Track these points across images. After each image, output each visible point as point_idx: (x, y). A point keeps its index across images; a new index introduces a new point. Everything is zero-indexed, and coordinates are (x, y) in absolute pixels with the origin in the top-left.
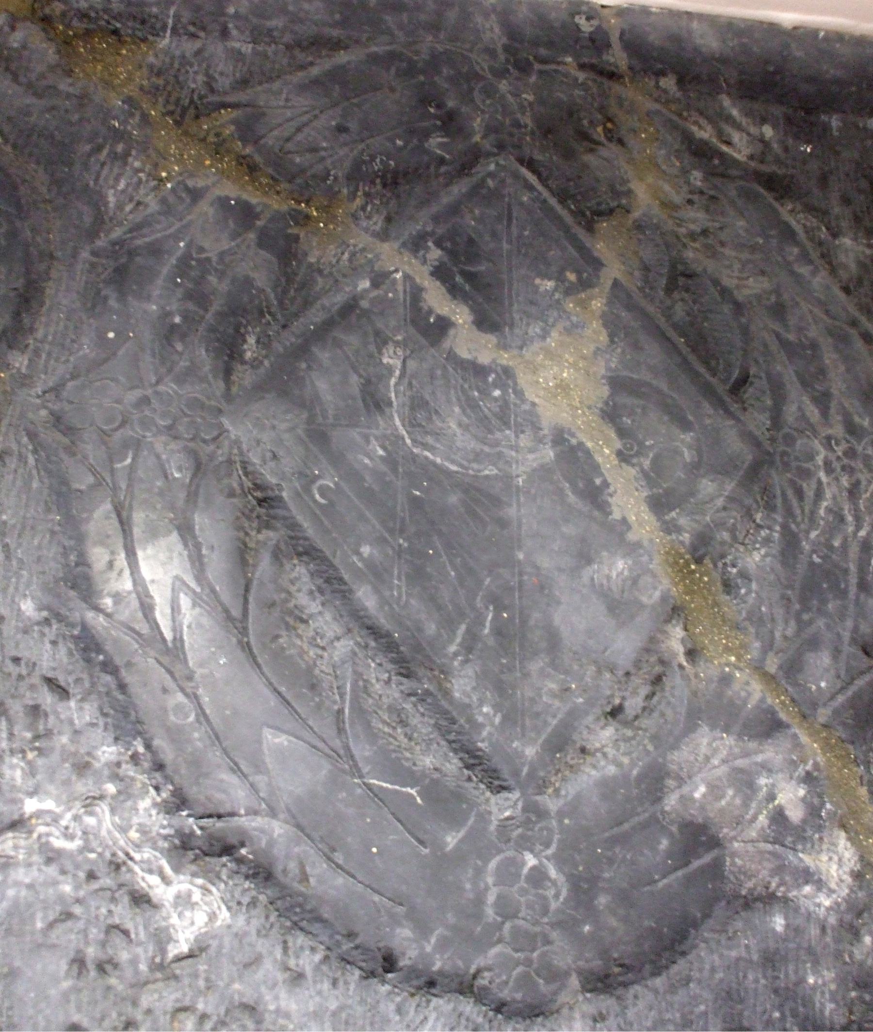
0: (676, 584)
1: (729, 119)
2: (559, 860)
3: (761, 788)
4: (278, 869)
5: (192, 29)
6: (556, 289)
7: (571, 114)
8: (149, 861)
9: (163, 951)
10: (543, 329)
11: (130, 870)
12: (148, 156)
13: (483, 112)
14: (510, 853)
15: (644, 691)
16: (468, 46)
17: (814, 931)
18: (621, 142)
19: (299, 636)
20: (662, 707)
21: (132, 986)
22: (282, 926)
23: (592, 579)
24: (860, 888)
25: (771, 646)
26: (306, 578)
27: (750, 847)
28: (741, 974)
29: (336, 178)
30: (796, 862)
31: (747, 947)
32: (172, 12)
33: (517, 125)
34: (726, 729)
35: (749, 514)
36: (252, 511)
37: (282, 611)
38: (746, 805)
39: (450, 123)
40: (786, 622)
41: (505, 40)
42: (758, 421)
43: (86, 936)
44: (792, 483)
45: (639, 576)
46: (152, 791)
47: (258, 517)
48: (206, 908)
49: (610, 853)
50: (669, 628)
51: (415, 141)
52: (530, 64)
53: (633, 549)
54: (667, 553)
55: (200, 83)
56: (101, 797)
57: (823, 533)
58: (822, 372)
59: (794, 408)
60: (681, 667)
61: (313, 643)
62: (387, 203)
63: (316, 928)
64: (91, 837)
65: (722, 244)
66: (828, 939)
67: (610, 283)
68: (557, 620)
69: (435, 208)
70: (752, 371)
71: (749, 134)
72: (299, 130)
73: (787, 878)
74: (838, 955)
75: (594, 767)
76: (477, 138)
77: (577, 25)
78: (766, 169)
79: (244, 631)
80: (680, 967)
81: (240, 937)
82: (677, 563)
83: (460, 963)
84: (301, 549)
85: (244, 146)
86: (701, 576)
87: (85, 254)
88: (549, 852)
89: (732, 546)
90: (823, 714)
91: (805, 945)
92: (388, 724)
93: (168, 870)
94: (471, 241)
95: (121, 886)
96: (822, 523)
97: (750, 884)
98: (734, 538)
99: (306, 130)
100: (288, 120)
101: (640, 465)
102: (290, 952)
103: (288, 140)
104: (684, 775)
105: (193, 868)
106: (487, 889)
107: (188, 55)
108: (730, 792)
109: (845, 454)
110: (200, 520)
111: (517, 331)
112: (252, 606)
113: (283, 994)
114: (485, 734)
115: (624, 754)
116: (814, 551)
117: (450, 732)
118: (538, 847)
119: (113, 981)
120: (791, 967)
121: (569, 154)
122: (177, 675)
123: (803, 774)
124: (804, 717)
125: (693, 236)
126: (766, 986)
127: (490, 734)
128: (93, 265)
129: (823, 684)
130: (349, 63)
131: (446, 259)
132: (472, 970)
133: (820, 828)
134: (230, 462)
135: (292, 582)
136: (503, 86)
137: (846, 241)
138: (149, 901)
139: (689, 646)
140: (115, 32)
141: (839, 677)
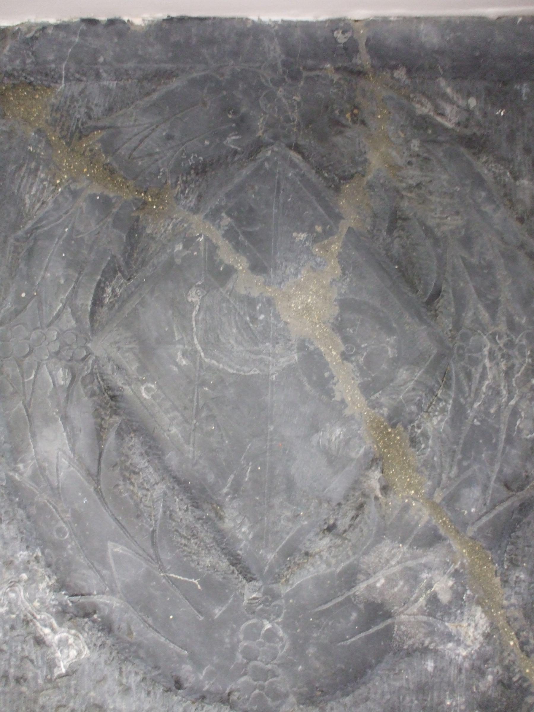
0: (377, 443)
1: (444, 96)
2: (286, 626)
3: (423, 580)
4: (115, 626)
5: (78, 76)
6: (306, 240)
7: (327, 107)
8: (44, 620)
9: (52, 673)
10: (296, 269)
11: (34, 625)
12: (50, 169)
13: (265, 113)
14: (254, 621)
15: (351, 514)
16: (258, 65)
17: (453, 671)
18: (363, 123)
19: (132, 484)
20: (361, 525)
21: (35, 692)
22: (119, 659)
23: (318, 442)
24: (488, 644)
25: (439, 483)
26: (138, 446)
27: (412, 619)
28: (401, 697)
29: (164, 173)
30: (442, 628)
31: (407, 680)
32: (64, 66)
33: (288, 120)
34: (403, 541)
35: (432, 392)
36: (107, 403)
37: (121, 469)
38: (411, 591)
39: (242, 124)
40: (451, 466)
41: (283, 57)
42: (446, 322)
43: (9, 663)
44: (464, 368)
45: (350, 439)
46: (47, 579)
47: (111, 407)
48: (76, 647)
49: (318, 621)
50: (370, 473)
51: (218, 140)
52: (299, 73)
53: (347, 420)
54: (372, 421)
55: (83, 113)
56: (19, 582)
57: (484, 403)
58: (494, 285)
59: (470, 314)
60: (376, 498)
61: (141, 487)
62: (199, 186)
63: (137, 661)
64: (13, 605)
65: (431, 193)
66: (463, 677)
67: (345, 231)
68: (293, 471)
69: (230, 187)
70: (444, 287)
71: (458, 106)
72: (142, 141)
73: (436, 639)
74: (468, 687)
75: (313, 565)
76: (260, 133)
77: (335, 39)
78: (468, 132)
79: (98, 483)
80: (362, 691)
81: (95, 665)
82: (378, 427)
83: (220, 687)
84: (135, 428)
85: (106, 158)
86: (395, 435)
87: (11, 240)
88: (280, 620)
89: (418, 414)
90: (471, 531)
91: (446, 679)
92: (185, 538)
93: (55, 625)
94: (251, 210)
95: (29, 633)
96: (483, 396)
97: (410, 642)
98: (420, 409)
99: (147, 141)
100: (135, 135)
101: (357, 362)
102: (124, 674)
103: (135, 149)
104: (370, 571)
105: (69, 623)
106: (239, 642)
107: (76, 94)
108: (401, 583)
109: (505, 345)
110: (75, 413)
111: (279, 272)
112: (103, 466)
113: (118, 700)
114: (242, 545)
115: (334, 557)
116: (476, 417)
117: (222, 543)
118: (272, 617)
119: (24, 689)
120: (435, 694)
121: (322, 138)
122: (59, 510)
123: (453, 571)
124: (458, 532)
125: (410, 188)
126: (417, 705)
127: (245, 545)
128: (16, 247)
129: (473, 510)
130: (176, 88)
131: (233, 224)
132: (228, 691)
133: (461, 607)
134: (92, 373)
135: (130, 449)
136: (280, 92)
137: (525, 182)
138: (44, 643)
139: (384, 484)
140: (30, 83)
141: (485, 504)
